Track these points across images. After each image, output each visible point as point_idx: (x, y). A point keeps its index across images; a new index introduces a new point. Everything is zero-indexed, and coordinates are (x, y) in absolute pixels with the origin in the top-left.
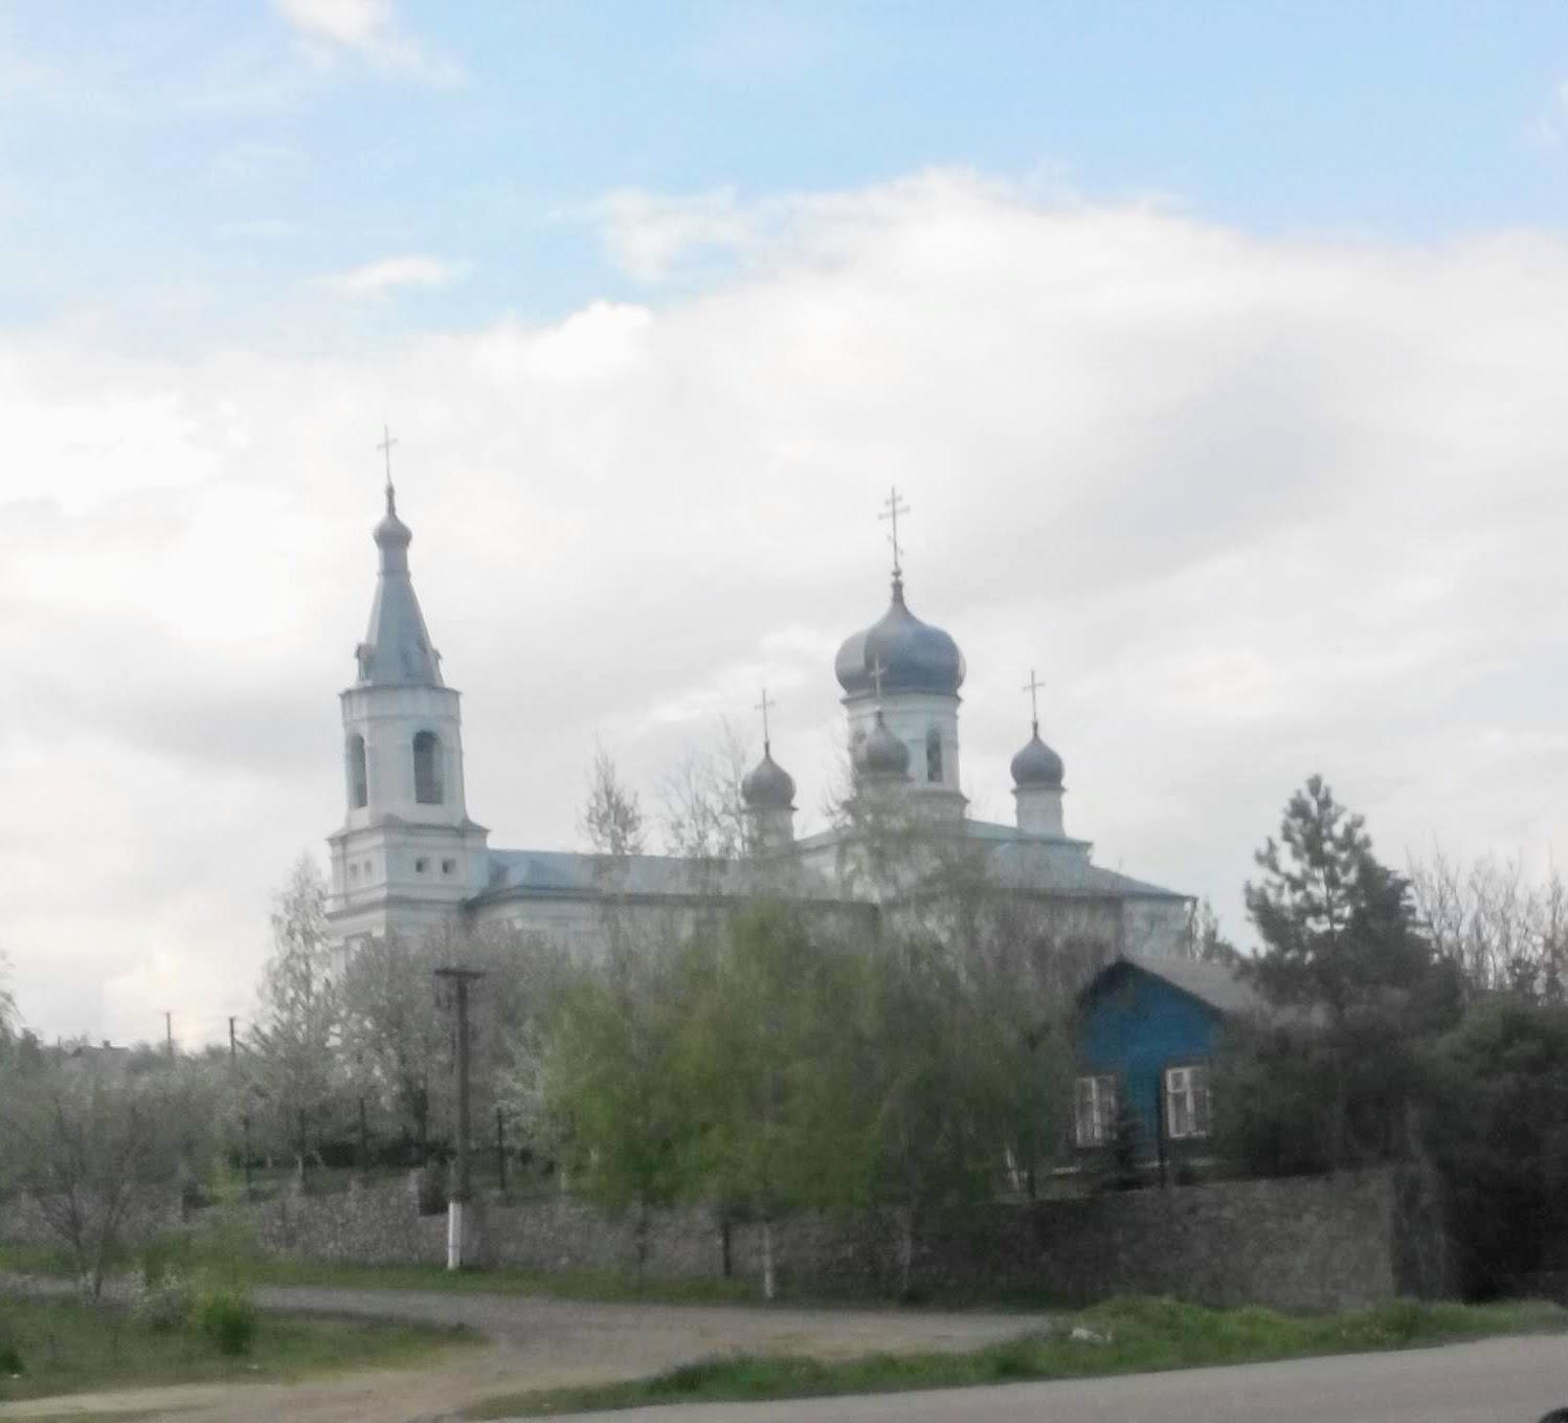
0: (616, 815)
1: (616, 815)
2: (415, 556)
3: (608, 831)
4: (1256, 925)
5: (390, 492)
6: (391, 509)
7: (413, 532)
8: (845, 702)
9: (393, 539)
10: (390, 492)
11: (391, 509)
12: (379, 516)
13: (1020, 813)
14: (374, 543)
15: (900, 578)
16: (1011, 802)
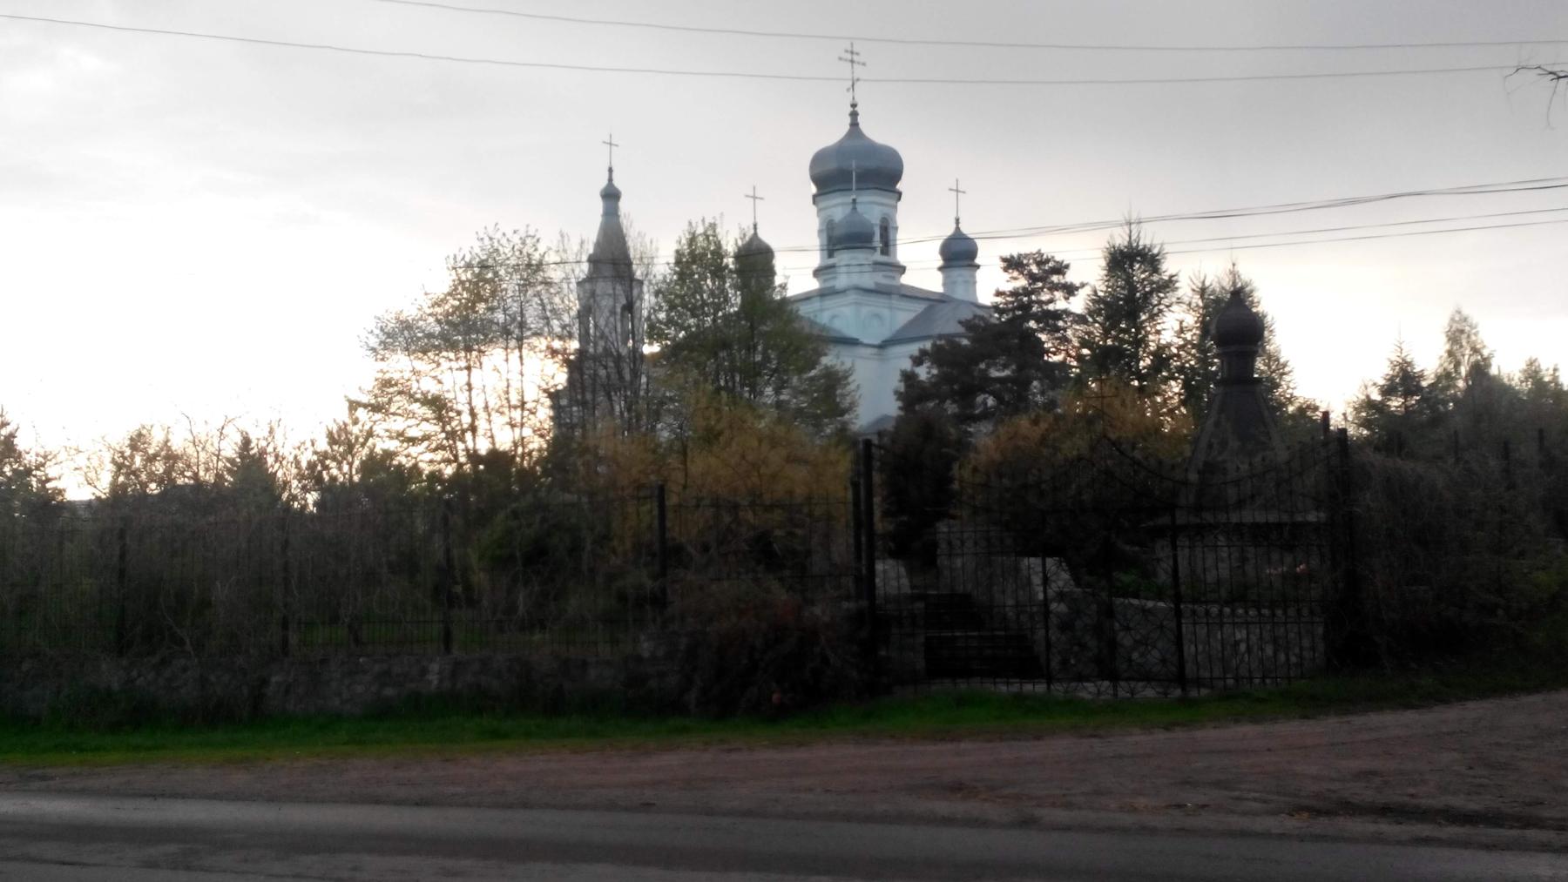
0: (613, 254)
1: (613, 254)
2: (624, 205)
3: (833, 456)
4: (821, 224)
5: (610, 170)
6: (610, 180)
7: (623, 193)
8: (940, 269)
9: (611, 196)
10: (610, 170)
11: (610, 180)
12: (604, 183)
13: (944, 285)
14: (600, 198)
15: (856, 109)
16: (939, 276)
